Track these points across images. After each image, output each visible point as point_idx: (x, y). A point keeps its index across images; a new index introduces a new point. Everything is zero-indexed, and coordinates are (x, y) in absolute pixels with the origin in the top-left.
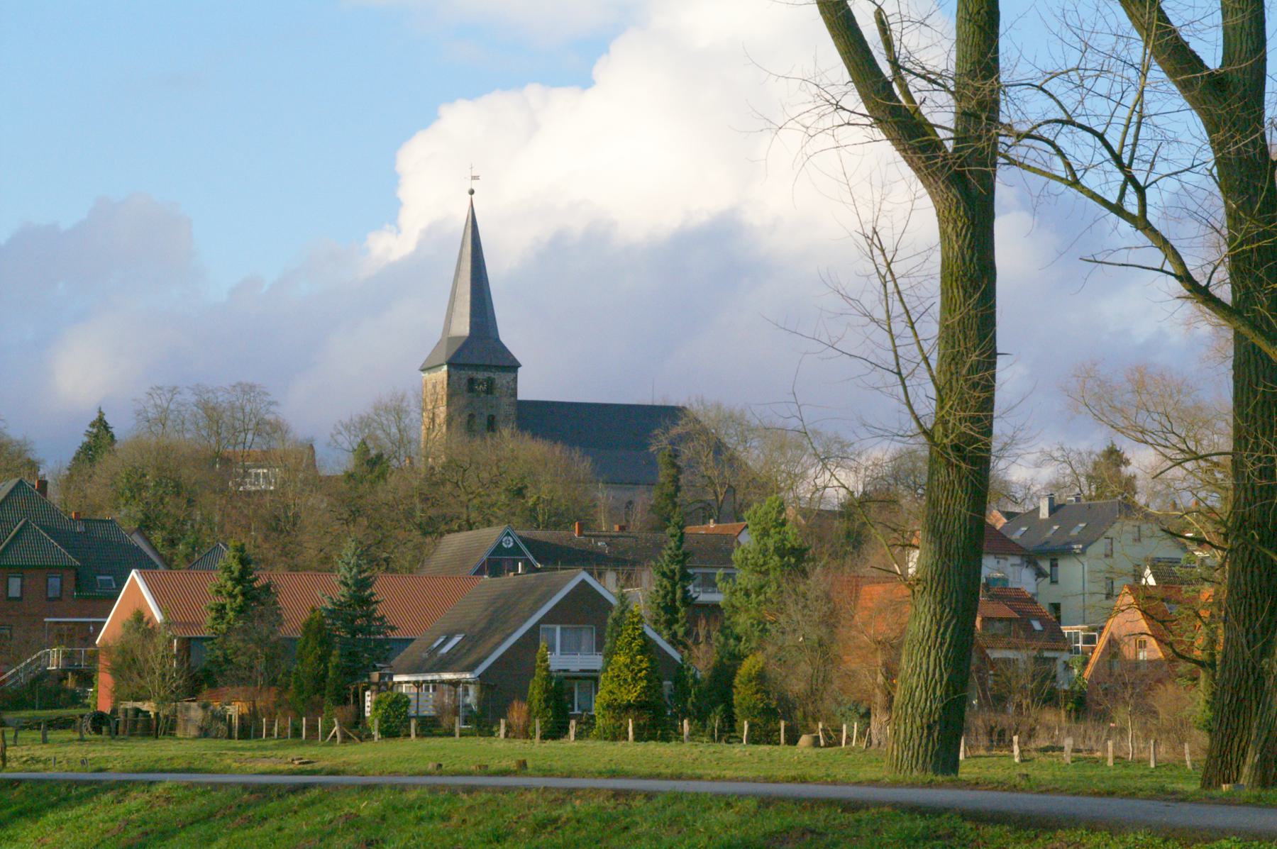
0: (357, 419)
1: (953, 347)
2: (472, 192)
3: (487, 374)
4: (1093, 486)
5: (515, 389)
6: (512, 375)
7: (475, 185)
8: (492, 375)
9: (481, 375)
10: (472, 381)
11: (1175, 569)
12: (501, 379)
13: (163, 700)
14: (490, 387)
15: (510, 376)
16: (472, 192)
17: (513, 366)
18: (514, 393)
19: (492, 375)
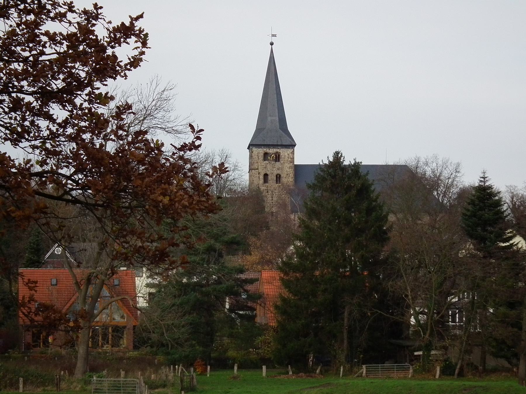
0: (469, 179)
1: (379, 371)
2: (272, 44)
3: (275, 150)
4: (39, 101)
5: (293, 158)
6: (291, 150)
7: (274, 40)
8: (278, 150)
9: (272, 151)
10: (266, 154)
11: (73, 71)
12: (284, 153)
13: (421, 307)
14: (277, 158)
15: (290, 151)
16: (272, 44)
17: (292, 145)
18: (292, 161)
19: (278, 150)
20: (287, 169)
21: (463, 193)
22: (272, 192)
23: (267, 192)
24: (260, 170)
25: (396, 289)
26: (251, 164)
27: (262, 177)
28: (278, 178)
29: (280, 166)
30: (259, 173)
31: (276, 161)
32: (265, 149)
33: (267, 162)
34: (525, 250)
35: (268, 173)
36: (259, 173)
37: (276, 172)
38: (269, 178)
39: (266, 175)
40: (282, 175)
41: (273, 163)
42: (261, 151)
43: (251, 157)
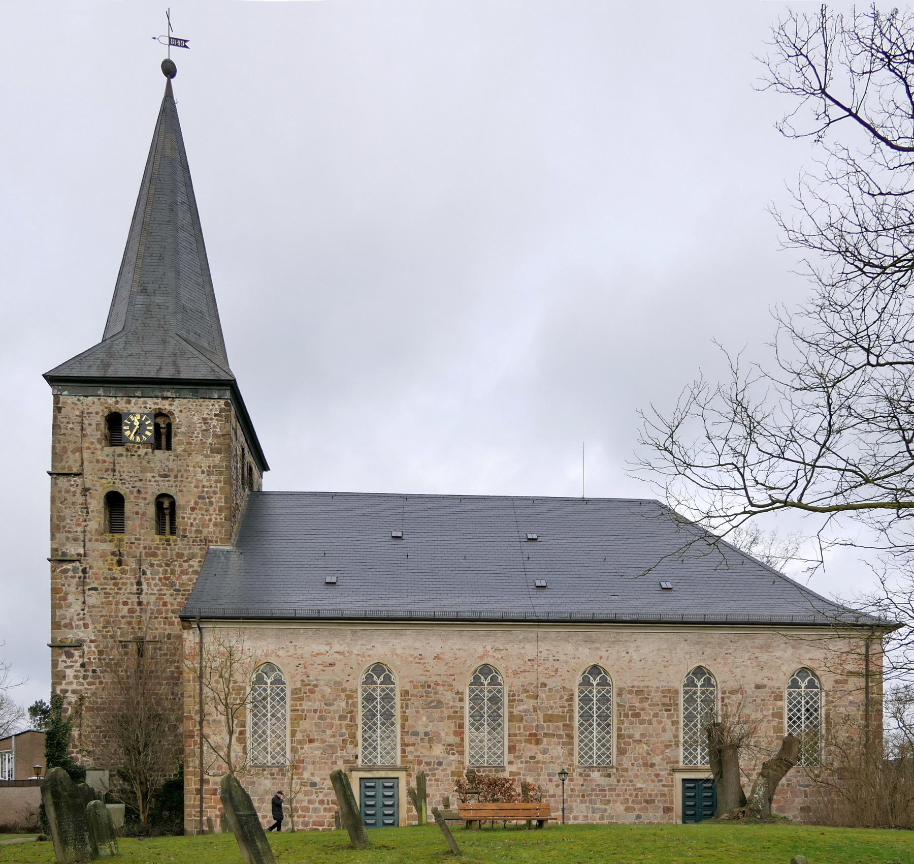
7: (177, 55)
9: (138, 410)
10: (114, 421)
16: (169, 70)
19: (165, 405)
20: (200, 476)
21: (164, 786)
22: (140, 562)
23: (120, 563)
24: (89, 479)
25: (66, 578)
26: (57, 455)
27: (97, 504)
28: (166, 511)
29: (171, 465)
30: (85, 490)
31: (158, 447)
32: (111, 401)
33: (119, 450)
34: (913, 746)
35: (122, 489)
36: (85, 490)
37: (153, 489)
38: (128, 507)
39: (114, 501)
40: (180, 501)
41: (142, 451)
42: (97, 405)
43: (57, 409)
